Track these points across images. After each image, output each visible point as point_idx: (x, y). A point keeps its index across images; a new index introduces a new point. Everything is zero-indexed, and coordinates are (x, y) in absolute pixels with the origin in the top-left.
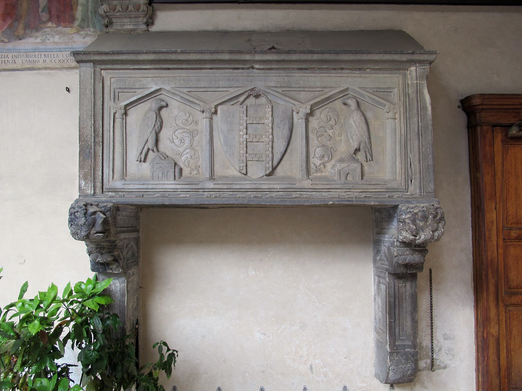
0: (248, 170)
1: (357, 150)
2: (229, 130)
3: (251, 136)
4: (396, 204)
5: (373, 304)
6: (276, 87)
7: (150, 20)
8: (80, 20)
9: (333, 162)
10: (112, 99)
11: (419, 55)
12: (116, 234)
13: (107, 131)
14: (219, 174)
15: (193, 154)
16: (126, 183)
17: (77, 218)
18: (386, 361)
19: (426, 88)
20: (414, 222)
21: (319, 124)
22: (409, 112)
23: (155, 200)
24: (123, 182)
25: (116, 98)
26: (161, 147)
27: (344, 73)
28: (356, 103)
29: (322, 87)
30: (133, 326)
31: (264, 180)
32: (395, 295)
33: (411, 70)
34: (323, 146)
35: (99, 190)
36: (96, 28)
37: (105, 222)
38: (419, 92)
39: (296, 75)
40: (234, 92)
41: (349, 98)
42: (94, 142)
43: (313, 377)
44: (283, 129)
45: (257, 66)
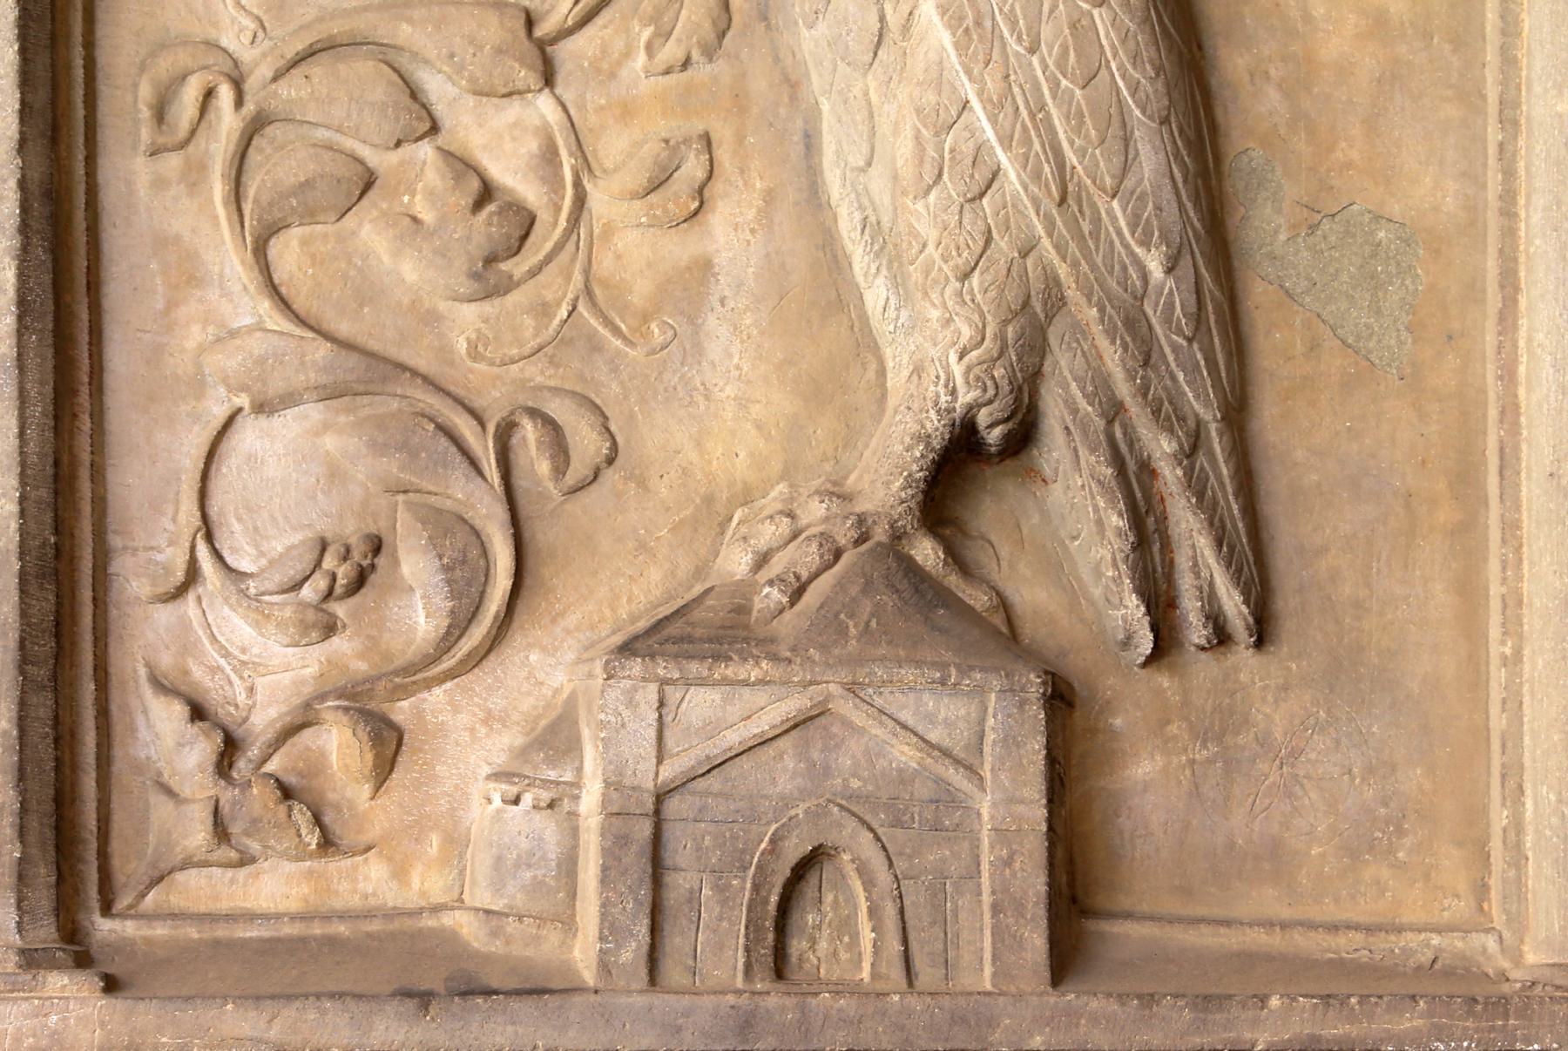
1: (963, 466)
9: (548, 665)
12: (1378, 312)
34: (367, 374)
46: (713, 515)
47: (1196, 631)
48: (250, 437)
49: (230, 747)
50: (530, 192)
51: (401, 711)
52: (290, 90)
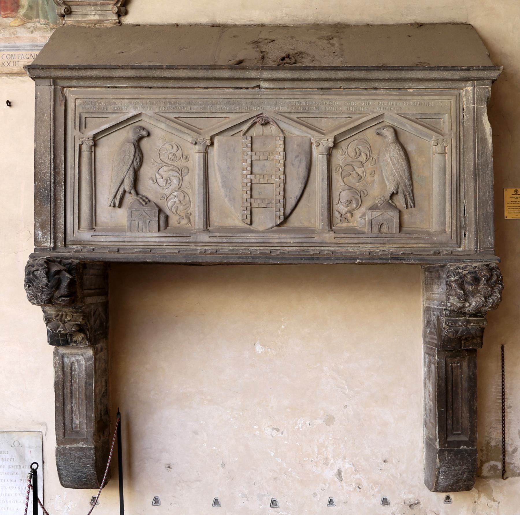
0: (253, 219)
1: (393, 195)
2: (229, 168)
3: (257, 176)
4: (444, 262)
5: (423, 391)
6: (290, 112)
7: (122, 9)
8: (26, 7)
9: (363, 209)
10: (78, 127)
11: (476, 72)
13: (71, 168)
14: (216, 224)
15: (182, 198)
16: (95, 234)
17: (37, 278)
18: (435, 462)
20: (461, 286)
21: (345, 160)
22: (464, 145)
23: (133, 256)
24: (92, 233)
25: (82, 125)
26: (142, 189)
27: (378, 95)
28: (393, 135)
29: (350, 113)
30: (101, 417)
31: (274, 232)
32: (446, 378)
33: (467, 91)
34: (351, 188)
35: (60, 243)
36: (48, 20)
37: (72, 284)
38: (476, 120)
39: (316, 97)
40: (234, 118)
41: (385, 127)
42: (54, 182)
43: (342, 486)
44: (298, 167)
45: (264, 85)
46: (375, 198)
47: (409, 207)
48: (342, 193)
49: (341, 215)
50: (362, 175)
51: (353, 212)
52: (345, 168)
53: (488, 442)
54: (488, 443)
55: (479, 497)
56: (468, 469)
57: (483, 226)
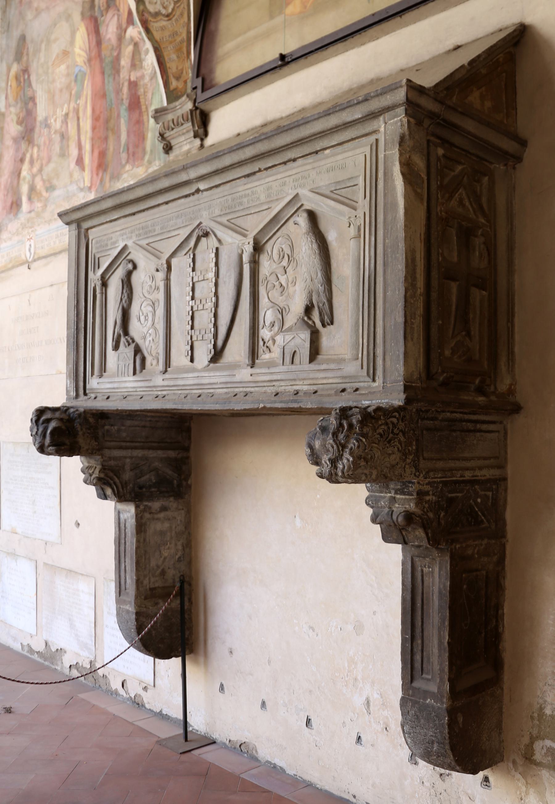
11: (376, 99)
19: (397, 164)
43: (370, 722)
53: (541, 707)
54: (541, 709)
55: (527, 793)
56: (436, 737)
57: (391, 345)
